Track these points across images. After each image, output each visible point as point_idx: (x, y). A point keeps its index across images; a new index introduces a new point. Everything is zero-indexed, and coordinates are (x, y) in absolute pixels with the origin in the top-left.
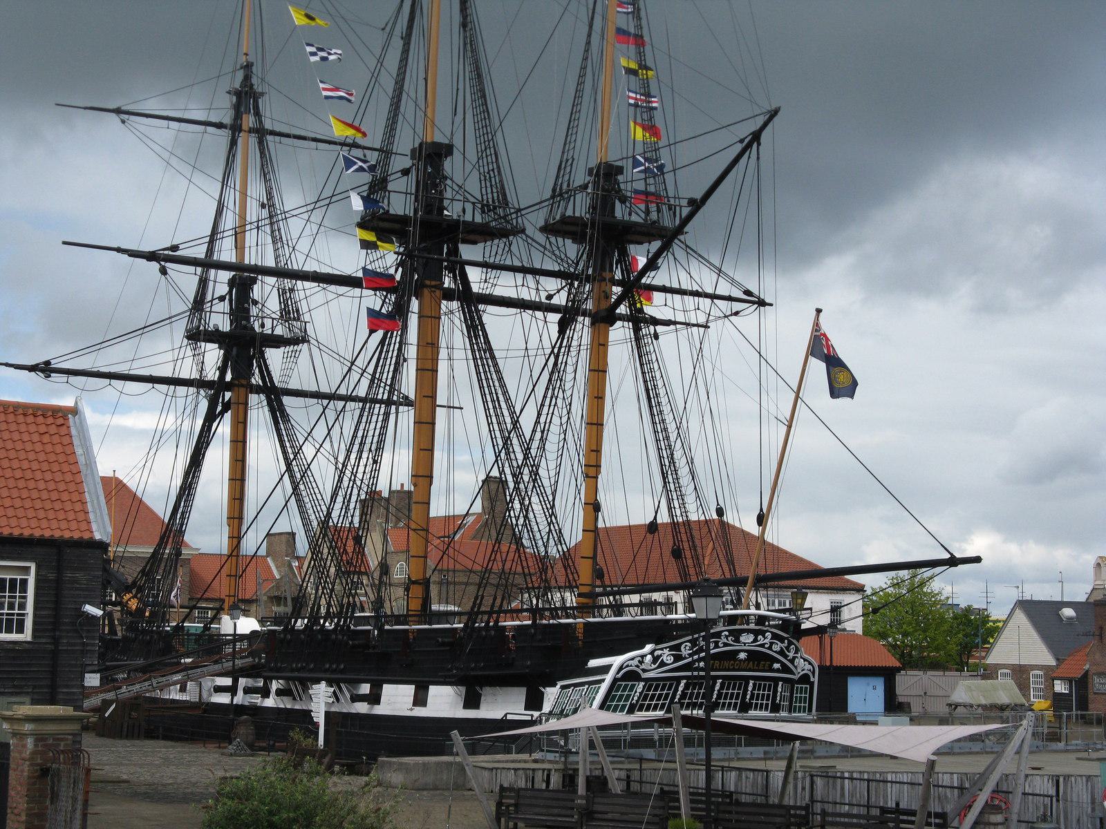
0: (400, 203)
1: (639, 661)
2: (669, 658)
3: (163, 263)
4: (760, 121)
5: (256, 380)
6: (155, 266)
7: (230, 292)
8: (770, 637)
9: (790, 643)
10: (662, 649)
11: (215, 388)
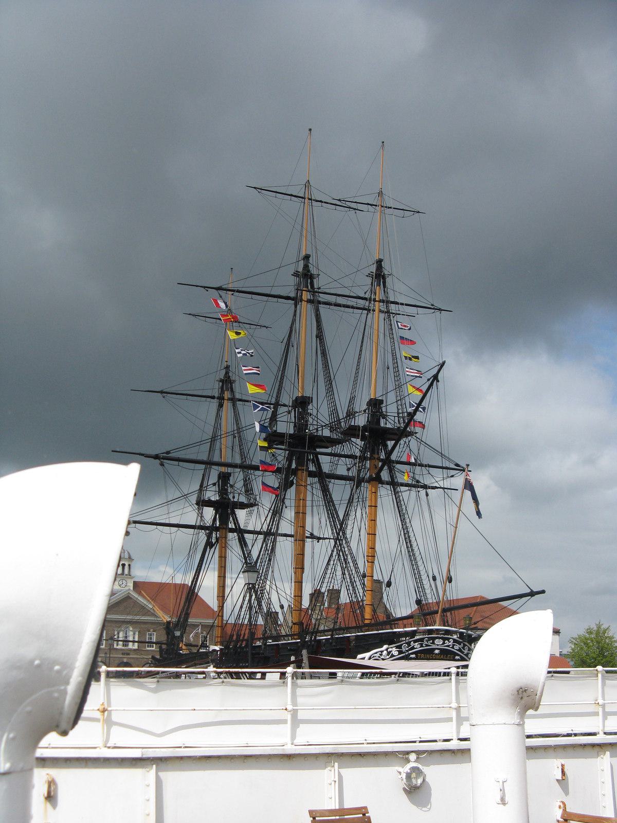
0: (285, 426)
1: (380, 654)
2: (395, 652)
3: (162, 460)
4: (437, 368)
5: (231, 525)
6: (158, 461)
7: (218, 481)
8: (452, 641)
9: (465, 645)
10: (392, 648)
11: (210, 529)
